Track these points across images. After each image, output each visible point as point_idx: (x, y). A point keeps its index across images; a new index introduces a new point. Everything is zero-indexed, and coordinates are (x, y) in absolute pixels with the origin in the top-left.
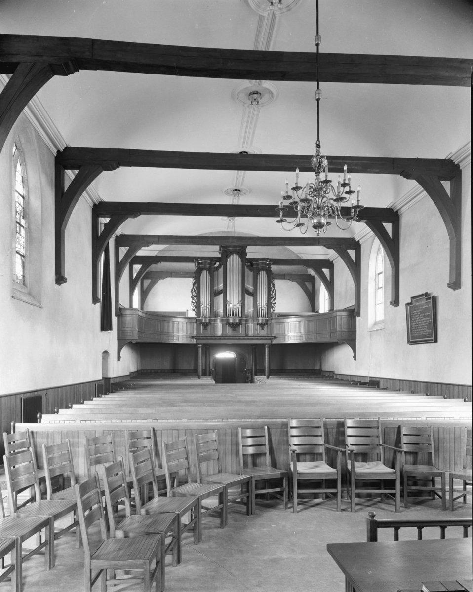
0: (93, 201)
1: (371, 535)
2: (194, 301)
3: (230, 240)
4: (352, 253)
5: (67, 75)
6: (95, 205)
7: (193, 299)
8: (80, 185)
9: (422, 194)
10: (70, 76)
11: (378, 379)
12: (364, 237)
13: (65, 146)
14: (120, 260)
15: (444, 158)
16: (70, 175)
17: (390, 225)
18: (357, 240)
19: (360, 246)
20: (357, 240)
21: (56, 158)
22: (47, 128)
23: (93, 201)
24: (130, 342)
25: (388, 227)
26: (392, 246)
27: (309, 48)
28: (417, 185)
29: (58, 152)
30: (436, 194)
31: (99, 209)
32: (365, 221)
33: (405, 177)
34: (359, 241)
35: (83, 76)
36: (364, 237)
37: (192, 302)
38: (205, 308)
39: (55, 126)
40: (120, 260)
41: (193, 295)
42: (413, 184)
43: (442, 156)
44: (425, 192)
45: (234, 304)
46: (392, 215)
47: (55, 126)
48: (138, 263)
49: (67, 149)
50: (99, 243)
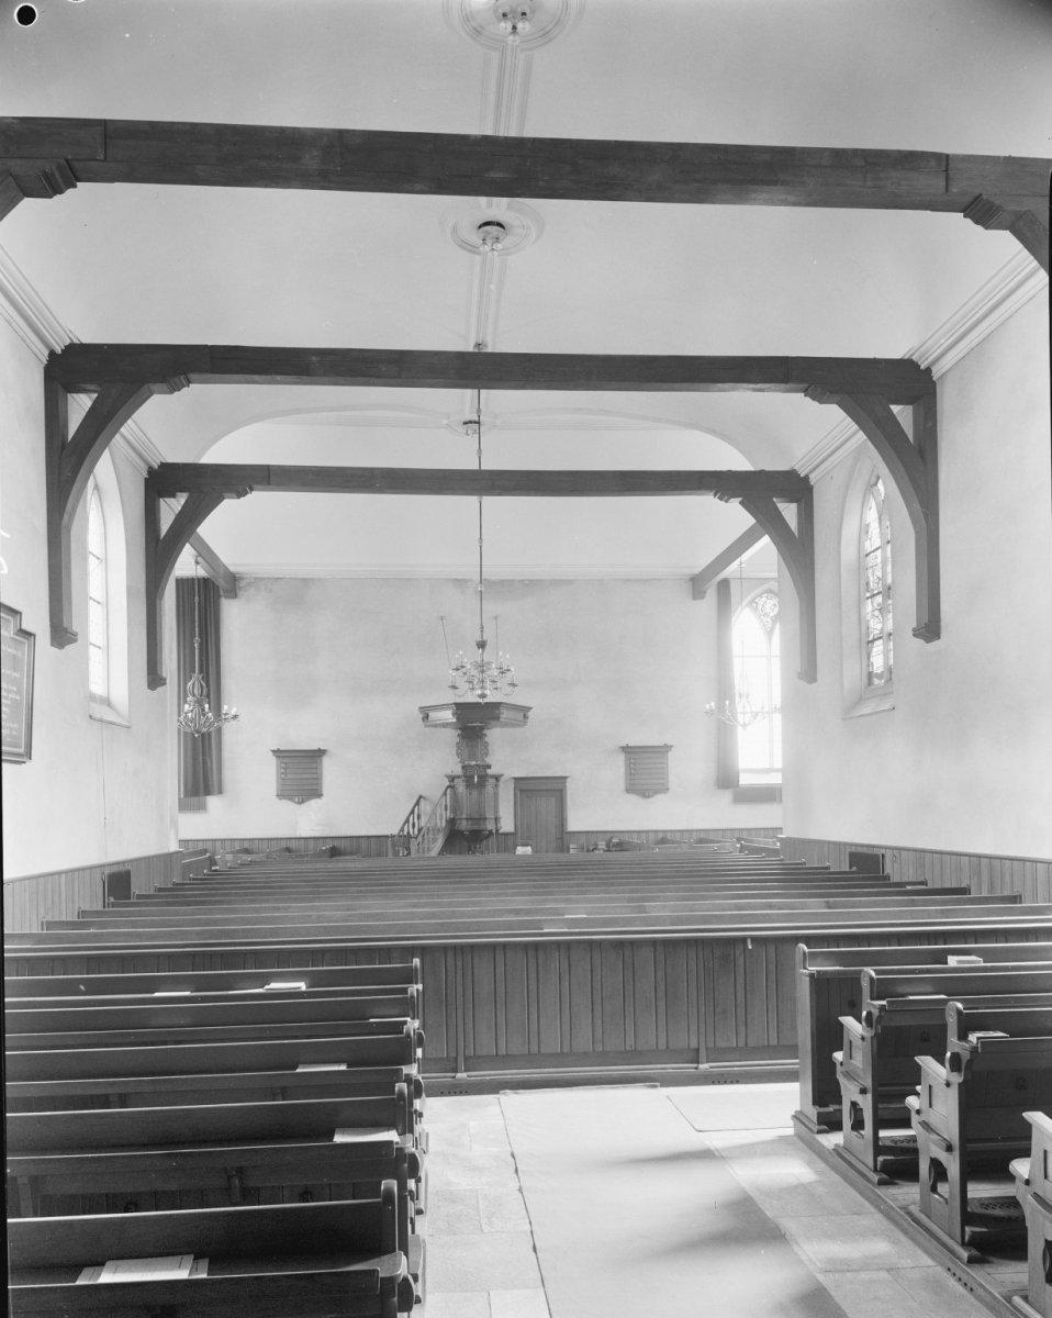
1: (75, 472)
4: (789, 511)
5: (51, 197)
6: (151, 471)
8: (101, 424)
9: (853, 440)
10: (58, 197)
11: (876, 851)
12: (817, 466)
13: (68, 342)
16: (80, 405)
17: (794, 506)
19: (810, 490)
20: (922, 367)
21: (146, 479)
22: (44, 330)
25: (903, 413)
26: (799, 551)
27: (487, 500)
28: (1021, 251)
29: (52, 354)
30: (882, 432)
31: (161, 480)
33: (977, 222)
35: (84, 194)
36: (817, 466)
39: (51, 313)
43: (895, 351)
44: (861, 433)
46: (797, 487)
47: (51, 313)
49: (164, 466)
50: (158, 551)
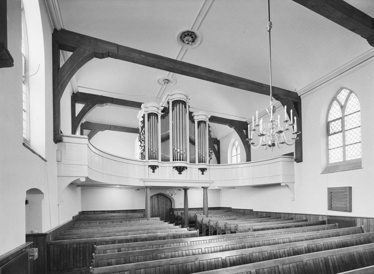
0: (73, 91)
2: (142, 145)
3: (191, 75)
7: (141, 143)
14: (77, 115)
15: (245, 121)
18: (299, 96)
20: (299, 96)
23: (73, 91)
24: (72, 184)
31: (77, 97)
32: (234, 127)
34: (300, 96)
37: (140, 146)
38: (154, 151)
40: (77, 115)
41: (141, 139)
42: (232, 130)
45: (181, 149)
48: (80, 102)
